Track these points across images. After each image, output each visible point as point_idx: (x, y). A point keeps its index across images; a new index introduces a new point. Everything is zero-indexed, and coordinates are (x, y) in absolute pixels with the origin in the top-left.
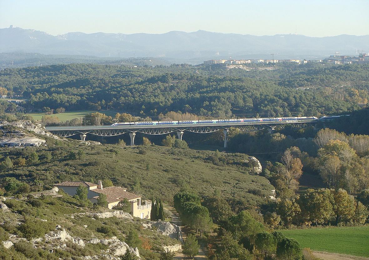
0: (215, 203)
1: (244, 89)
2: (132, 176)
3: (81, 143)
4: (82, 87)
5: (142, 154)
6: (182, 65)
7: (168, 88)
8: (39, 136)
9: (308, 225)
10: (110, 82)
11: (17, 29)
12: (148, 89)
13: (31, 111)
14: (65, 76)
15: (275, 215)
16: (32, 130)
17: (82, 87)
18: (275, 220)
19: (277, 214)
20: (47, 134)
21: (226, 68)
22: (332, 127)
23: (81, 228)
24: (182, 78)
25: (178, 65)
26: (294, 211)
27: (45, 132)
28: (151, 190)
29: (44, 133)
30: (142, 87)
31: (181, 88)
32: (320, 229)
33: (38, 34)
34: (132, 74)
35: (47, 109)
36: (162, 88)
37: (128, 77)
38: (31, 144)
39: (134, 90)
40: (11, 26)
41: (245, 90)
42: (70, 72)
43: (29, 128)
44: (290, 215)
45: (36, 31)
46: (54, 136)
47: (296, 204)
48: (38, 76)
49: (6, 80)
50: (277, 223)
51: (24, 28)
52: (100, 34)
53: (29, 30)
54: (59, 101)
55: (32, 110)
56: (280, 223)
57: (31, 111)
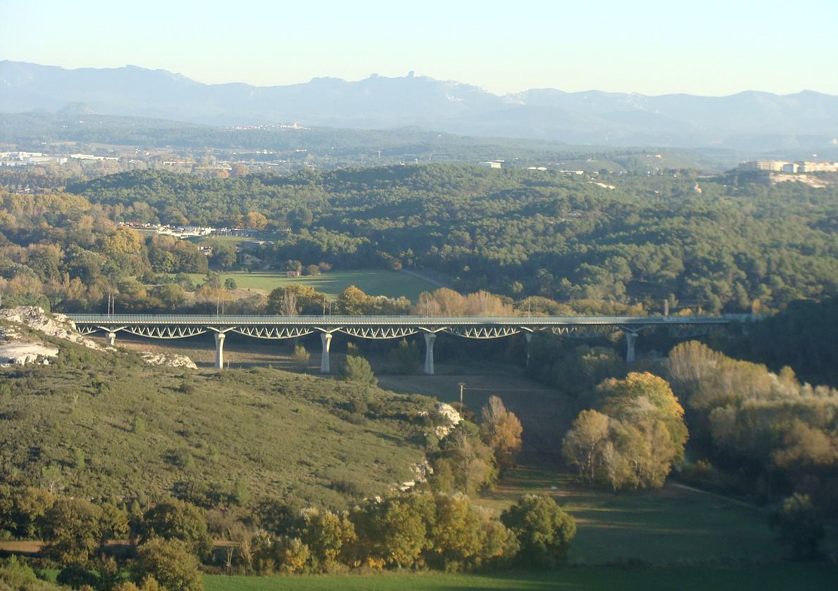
0: (168, 514)
1: (687, 237)
2: (82, 444)
3: (145, 356)
4: (402, 217)
5: (185, 392)
6: (682, 171)
7: (551, 229)
8: (49, 341)
9: (376, 567)
10: (462, 208)
11: (423, 79)
12: (509, 229)
13: (268, 267)
14: (405, 189)
15: (297, 542)
16: (40, 327)
17: (402, 217)
18: (296, 555)
19: (304, 542)
20: (71, 336)
21: (769, 181)
22: (704, 339)
23: (483, 509)
24: (591, 208)
25: (673, 171)
26: (341, 538)
27: (68, 332)
28: (104, 477)
29: (63, 335)
30: (496, 224)
31: (579, 228)
32: (400, 575)
33: (465, 91)
34: (537, 192)
35: (294, 264)
36: (540, 227)
37: (527, 197)
38: (11, 358)
39: (478, 231)
40: (411, 73)
41: (689, 240)
42: (423, 181)
43: (33, 324)
44: (331, 546)
45: (461, 86)
46: (86, 341)
47: (346, 522)
48: (360, 189)
49: (286, 196)
50: (300, 562)
51: (437, 78)
52: (595, 95)
53: (448, 82)
54: (325, 248)
55: (271, 266)
56: (309, 562)
57: (268, 267)
